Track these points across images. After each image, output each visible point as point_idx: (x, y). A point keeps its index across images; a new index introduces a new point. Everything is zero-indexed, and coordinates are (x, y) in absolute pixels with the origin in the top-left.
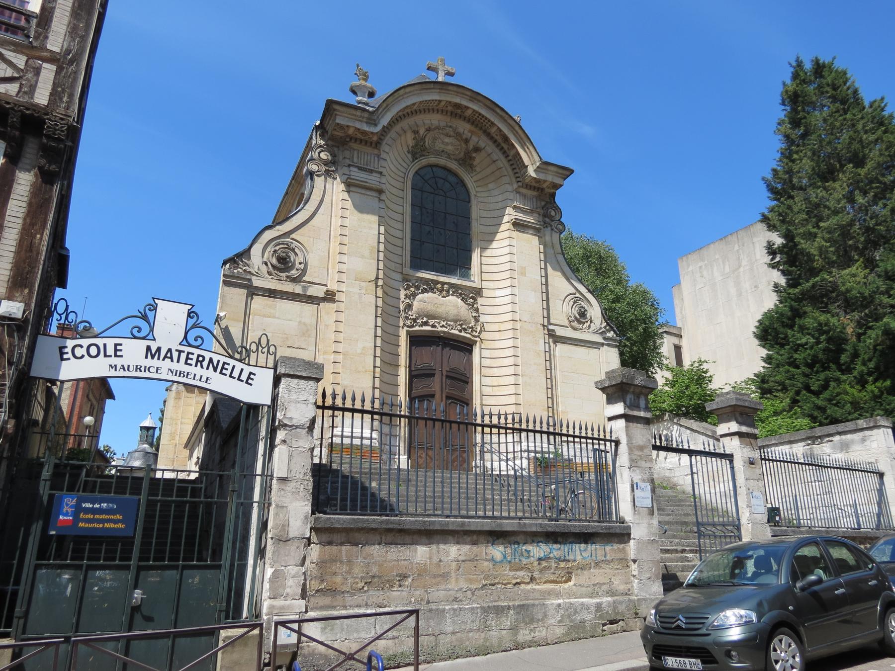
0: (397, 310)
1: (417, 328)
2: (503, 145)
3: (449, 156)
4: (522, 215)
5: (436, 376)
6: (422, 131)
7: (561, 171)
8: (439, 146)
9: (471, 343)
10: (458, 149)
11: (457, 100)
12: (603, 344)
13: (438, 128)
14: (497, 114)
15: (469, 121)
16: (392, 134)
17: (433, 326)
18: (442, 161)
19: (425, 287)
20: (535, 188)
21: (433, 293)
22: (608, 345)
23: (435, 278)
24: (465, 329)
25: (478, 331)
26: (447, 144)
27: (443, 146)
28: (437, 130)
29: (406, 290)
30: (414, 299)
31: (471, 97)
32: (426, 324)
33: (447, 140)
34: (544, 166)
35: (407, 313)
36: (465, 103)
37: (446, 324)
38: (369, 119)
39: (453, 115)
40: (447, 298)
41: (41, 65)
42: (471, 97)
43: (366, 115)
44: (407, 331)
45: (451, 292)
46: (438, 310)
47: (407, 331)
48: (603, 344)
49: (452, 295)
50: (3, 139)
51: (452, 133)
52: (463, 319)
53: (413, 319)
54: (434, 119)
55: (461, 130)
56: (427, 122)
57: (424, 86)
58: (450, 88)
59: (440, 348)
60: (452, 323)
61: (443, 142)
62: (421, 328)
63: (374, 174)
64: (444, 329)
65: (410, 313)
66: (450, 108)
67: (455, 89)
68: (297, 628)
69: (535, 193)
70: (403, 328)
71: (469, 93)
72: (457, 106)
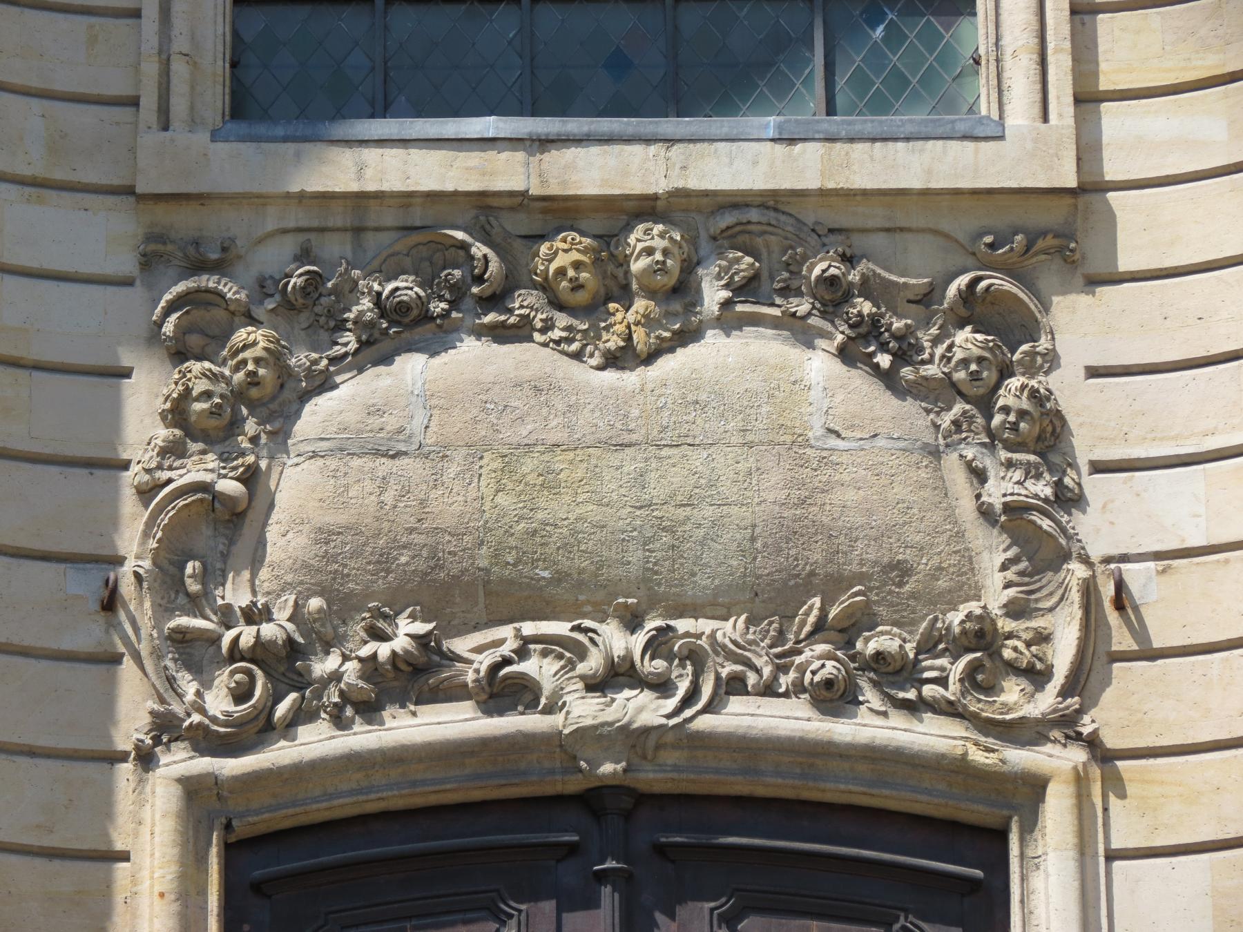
0: (85, 585)
5: (514, 919)
9: (977, 812)
19: (406, 287)
21: (502, 334)
25: (1062, 656)
29: (179, 354)
30: (281, 437)
35: (195, 605)
37: (655, 646)
40: (667, 365)
41: (1120, 569)
44: (192, 788)
45: (713, 295)
46: (553, 508)
47: (192, 788)
49: (729, 321)
52: (863, 555)
53: (261, 654)
59: (549, 906)
60: (729, 630)
65: (236, 594)
70: (146, 759)
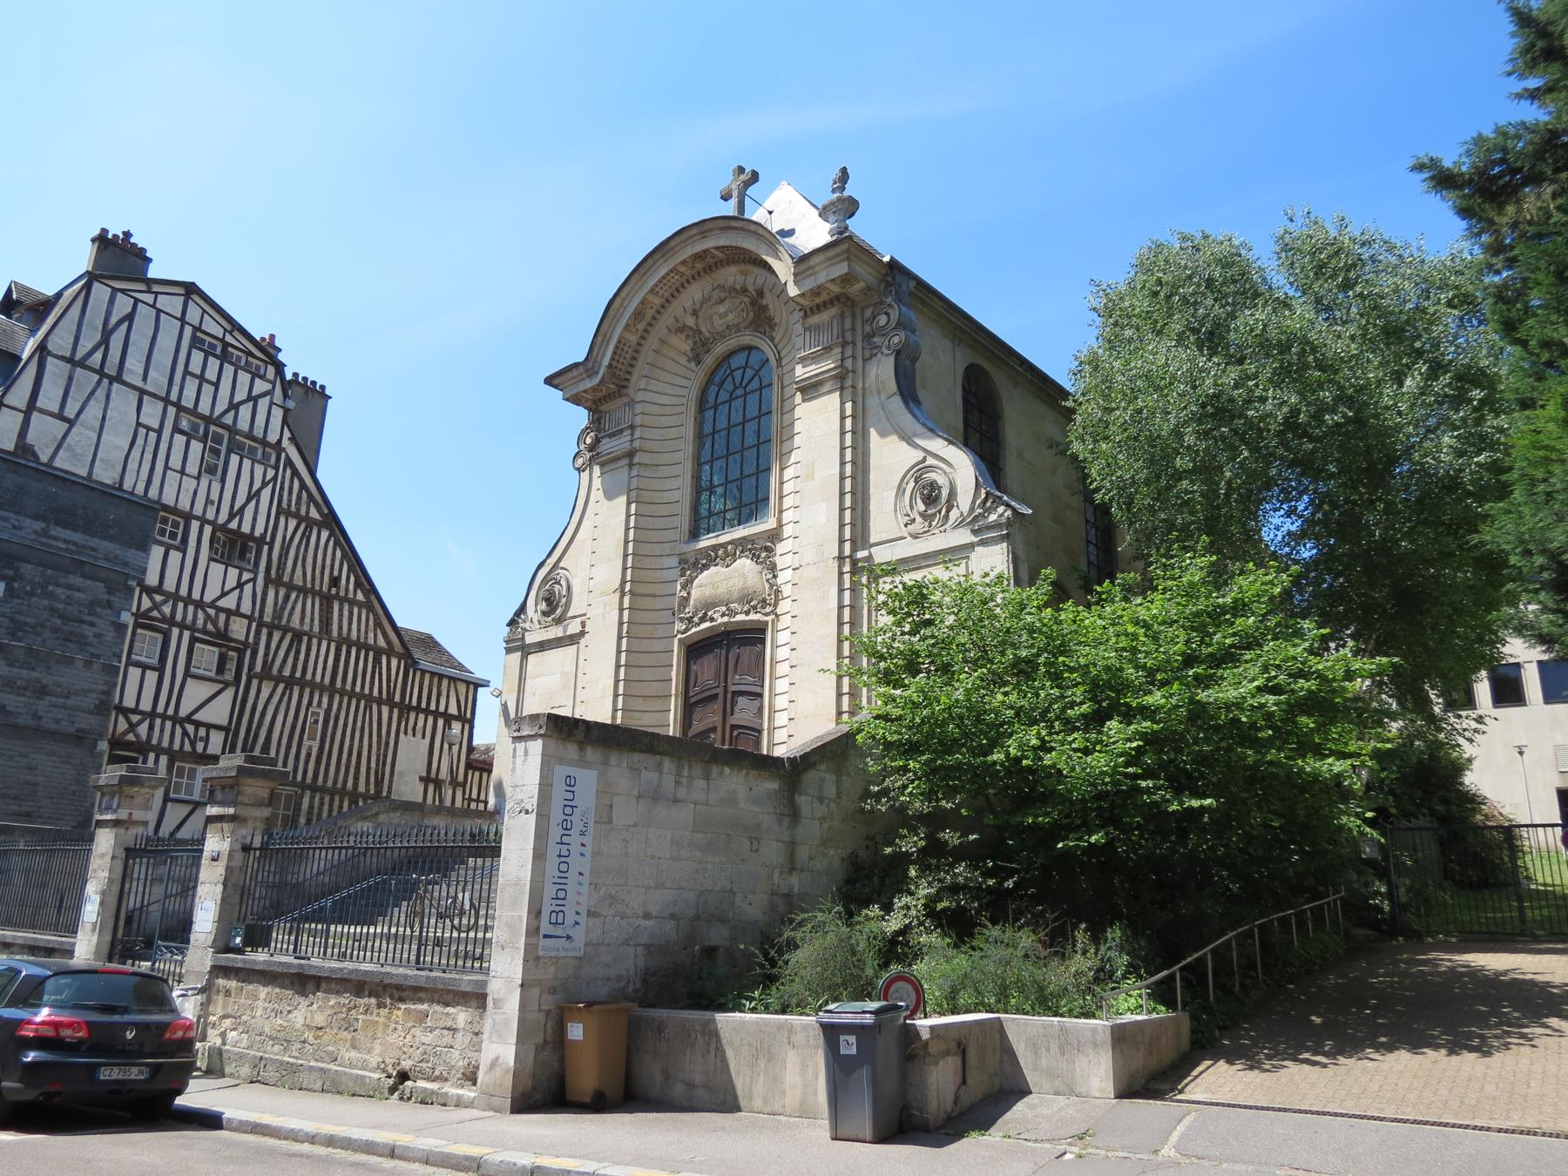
1: (694, 630)
2: (648, 318)
3: (737, 328)
4: (814, 367)
6: (690, 321)
7: (831, 253)
8: (719, 323)
10: (742, 310)
11: (689, 251)
12: (972, 546)
13: (704, 301)
14: (736, 228)
15: (728, 263)
16: (647, 355)
17: (712, 619)
18: (732, 343)
20: (824, 306)
22: (983, 543)
23: (714, 542)
24: (755, 608)
26: (726, 314)
27: (723, 321)
28: (705, 306)
31: (700, 233)
32: (703, 620)
33: (722, 309)
34: (803, 266)
36: (698, 248)
38: (587, 371)
39: (709, 269)
42: (700, 233)
43: (581, 369)
48: (972, 546)
50: (1548, 897)
51: (723, 295)
54: (695, 292)
55: (731, 282)
56: (689, 304)
57: (642, 270)
58: (672, 243)
61: (721, 316)
62: (698, 629)
63: (625, 433)
64: (726, 619)
66: (699, 266)
67: (678, 240)
68: (89, 362)
69: (834, 311)
71: (694, 231)
72: (698, 257)
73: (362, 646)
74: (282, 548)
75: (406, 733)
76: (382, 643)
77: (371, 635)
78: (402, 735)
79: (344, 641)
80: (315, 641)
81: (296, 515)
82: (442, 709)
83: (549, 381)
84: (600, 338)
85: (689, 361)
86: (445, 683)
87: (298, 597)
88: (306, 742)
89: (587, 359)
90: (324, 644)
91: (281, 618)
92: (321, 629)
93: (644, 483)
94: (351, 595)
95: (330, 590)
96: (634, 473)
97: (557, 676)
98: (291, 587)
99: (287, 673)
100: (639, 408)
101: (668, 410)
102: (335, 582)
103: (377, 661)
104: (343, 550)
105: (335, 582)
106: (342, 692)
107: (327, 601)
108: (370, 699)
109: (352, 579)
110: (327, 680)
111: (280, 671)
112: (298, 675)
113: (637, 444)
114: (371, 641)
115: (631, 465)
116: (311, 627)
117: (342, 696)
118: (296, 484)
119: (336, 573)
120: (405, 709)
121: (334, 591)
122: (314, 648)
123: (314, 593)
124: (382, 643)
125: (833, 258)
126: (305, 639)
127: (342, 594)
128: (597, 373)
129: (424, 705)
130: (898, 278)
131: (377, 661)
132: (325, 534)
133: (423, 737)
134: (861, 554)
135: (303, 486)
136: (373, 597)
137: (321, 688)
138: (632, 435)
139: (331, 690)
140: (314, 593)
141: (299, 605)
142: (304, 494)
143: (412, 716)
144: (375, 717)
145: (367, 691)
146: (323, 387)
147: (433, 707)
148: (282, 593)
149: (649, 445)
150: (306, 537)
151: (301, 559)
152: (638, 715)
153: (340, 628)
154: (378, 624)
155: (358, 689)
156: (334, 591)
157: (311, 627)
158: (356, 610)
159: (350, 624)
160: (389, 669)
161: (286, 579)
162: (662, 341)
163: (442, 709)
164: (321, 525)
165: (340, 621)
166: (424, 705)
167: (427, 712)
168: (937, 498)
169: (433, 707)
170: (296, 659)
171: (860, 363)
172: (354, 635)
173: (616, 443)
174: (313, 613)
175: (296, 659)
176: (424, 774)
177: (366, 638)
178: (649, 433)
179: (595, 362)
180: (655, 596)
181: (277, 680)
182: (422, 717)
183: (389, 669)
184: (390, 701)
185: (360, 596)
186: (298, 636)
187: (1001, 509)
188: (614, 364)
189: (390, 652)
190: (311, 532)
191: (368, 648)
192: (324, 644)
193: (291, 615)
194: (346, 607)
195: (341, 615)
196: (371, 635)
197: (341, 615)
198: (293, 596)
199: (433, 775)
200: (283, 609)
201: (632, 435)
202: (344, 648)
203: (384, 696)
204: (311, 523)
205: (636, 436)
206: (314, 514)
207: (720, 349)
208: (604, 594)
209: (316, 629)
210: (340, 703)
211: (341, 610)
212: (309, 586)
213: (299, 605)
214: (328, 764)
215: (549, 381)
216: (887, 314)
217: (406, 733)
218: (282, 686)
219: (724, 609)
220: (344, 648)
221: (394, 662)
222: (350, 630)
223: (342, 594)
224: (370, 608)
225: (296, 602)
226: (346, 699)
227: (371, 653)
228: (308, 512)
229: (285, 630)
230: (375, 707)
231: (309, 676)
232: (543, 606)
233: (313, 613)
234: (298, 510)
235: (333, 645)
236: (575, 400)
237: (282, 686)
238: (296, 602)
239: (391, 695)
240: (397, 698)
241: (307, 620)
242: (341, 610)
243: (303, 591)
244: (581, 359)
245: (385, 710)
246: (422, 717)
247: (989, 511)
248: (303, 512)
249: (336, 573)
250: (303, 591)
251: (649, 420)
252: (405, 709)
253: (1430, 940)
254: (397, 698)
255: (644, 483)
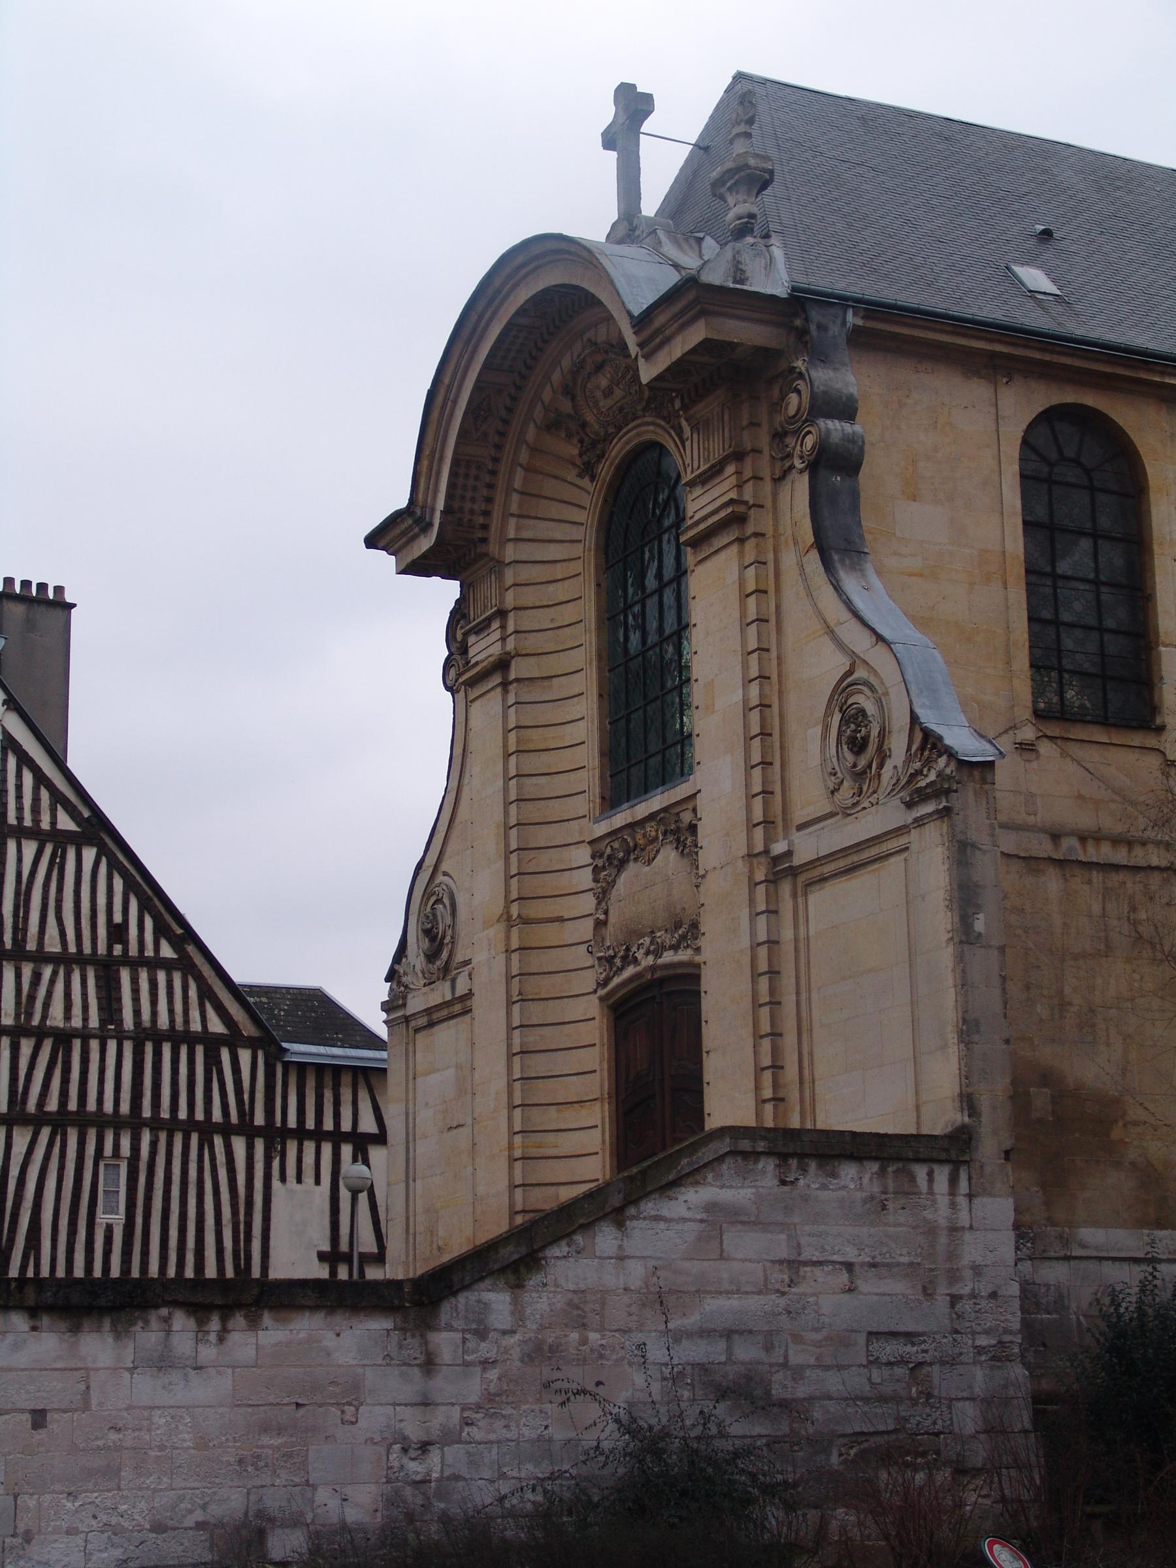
1: (616, 981)
44: (601, 999)
73: (180, 1038)
74: (17, 893)
75: (283, 1179)
76: (216, 1026)
77: (195, 1014)
78: (276, 1183)
79: (146, 1035)
80: (94, 1044)
81: (35, 833)
82: (346, 1126)
83: (372, 541)
84: (425, 463)
85: (580, 476)
86: (346, 1079)
87: (55, 973)
88: (102, 1218)
89: (412, 501)
90: (112, 1046)
91: (30, 1015)
92: (103, 1022)
93: (532, 715)
94: (149, 952)
95: (110, 948)
96: (511, 699)
97: (452, 1071)
98: (41, 957)
99: (52, 1105)
100: (509, 577)
101: (559, 571)
102: (118, 933)
103: (213, 1061)
104: (125, 875)
105: (118, 933)
106: (156, 1124)
107: (107, 971)
108: (207, 1130)
109: (149, 923)
110: (125, 1108)
111: (42, 1102)
112: (73, 1106)
113: (510, 645)
114: (196, 1026)
115: (505, 685)
116: (85, 1019)
117: (154, 1130)
118: (28, 778)
119: (118, 918)
120: (276, 1136)
121: (118, 949)
122: (95, 1056)
123: (81, 960)
124: (216, 1026)
125: (682, 312)
126: (77, 1044)
127: (133, 951)
128: (431, 525)
129: (310, 1124)
130: (815, 315)
131: (213, 1061)
132: (89, 854)
133: (318, 1182)
134: (779, 848)
135: (40, 779)
136: (191, 949)
137: (116, 1122)
138: (503, 627)
139: (135, 1123)
140: (81, 960)
141: (60, 987)
142: (45, 795)
143: (292, 1148)
144: (221, 1158)
145: (200, 1116)
146: (59, 590)
147: (328, 1125)
148: (27, 970)
149: (532, 643)
150: (57, 864)
151: (52, 906)
152: (551, 1137)
153: (137, 1013)
154: (206, 993)
155: (183, 1115)
156: (118, 949)
157: (85, 1019)
158: (161, 976)
159: (154, 1002)
160: (236, 1070)
161: (31, 946)
162: (535, 450)
163: (346, 1126)
164: (78, 840)
165: (136, 999)
166: (310, 1124)
167: (319, 1135)
168: (865, 740)
169: (328, 1125)
170: (65, 1081)
171: (767, 487)
172: (163, 1021)
173: (716, 492)
174: (85, 995)
175: (65, 1081)
176: (326, 1247)
177: (187, 1022)
178: (530, 620)
179: (423, 507)
180: (561, 920)
181: (37, 1121)
182: (309, 1147)
183: (236, 1070)
184: (248, 1131)
185: (167, 951)
186: (63, 1039)
187: (942, 761)
188: (456, 504)
189: (234, 1039)
190: (64, 858)
191: (191, 1039)
192: (112, 1046)
193: (46, 1005)
194: (144, 976)
195: (136, 991)
196: (195, 1014)
197: (136, 991)
198: (47, 972)
199: (344, 1247)
200: (32, 998)
201: (503, 627)
202: (149, 1048)
203: (234, 1118)
204: (60, 839)
205: (511, 628)
206: (66, 823)
207: (618, 450)
208: (487, 925)
209: (94, 1022)
210: (154, 1145)
211: (135, 981)
212: (72, 949)
213: (60, 987)
214: (145, 1253)
215: (372, 541)
216: (799, 392)
217: (283, 1179)
218: (46, 1132)
219: (647, 940)
220: (149, 1048)
221: (245, 1056)
222: (154, 1014)
223: (133, 951)
224: (185, 965)
225: (52, 982)
226: (163, 1137)
227: (200, 1050)
228: (54, 822)
229: (40, 1034)
230: (218, 1141)
231: (92, 1106)
232: (426, 943)
233: (85, 995)
234: (36, 821)
235: (128, 1047)
236: (416, 568)
237: (46, 1132)
238: (52, 982)
239: (246, 1114)
240: (259, 1119)
241: (77, 1010)
242: (135, 981)
243: (63, 960)
244: (403, 503)
245: (239, 1145)
246: (309, 1147)
247: (928, 763)
248: (45, 825)
249: (118, 918)
250: (63, 960)
251: (529, 596)
252: (276, 1136)
253: (968, 1508)
254: (259, 1119)
255: (532, 715)
